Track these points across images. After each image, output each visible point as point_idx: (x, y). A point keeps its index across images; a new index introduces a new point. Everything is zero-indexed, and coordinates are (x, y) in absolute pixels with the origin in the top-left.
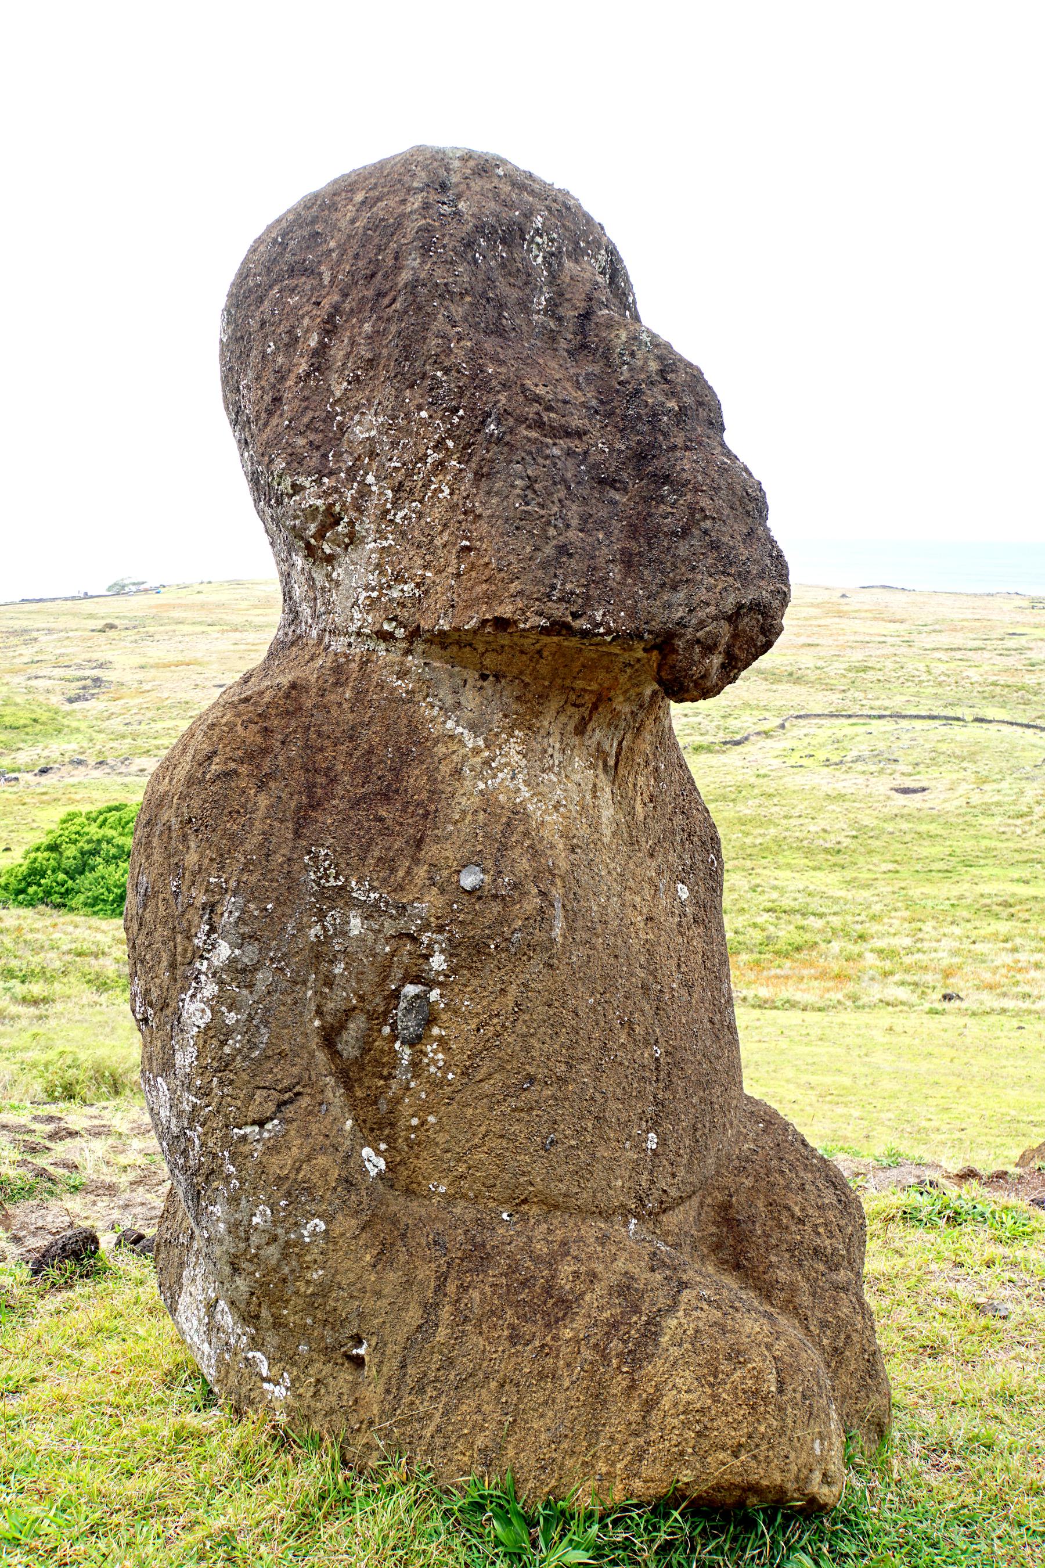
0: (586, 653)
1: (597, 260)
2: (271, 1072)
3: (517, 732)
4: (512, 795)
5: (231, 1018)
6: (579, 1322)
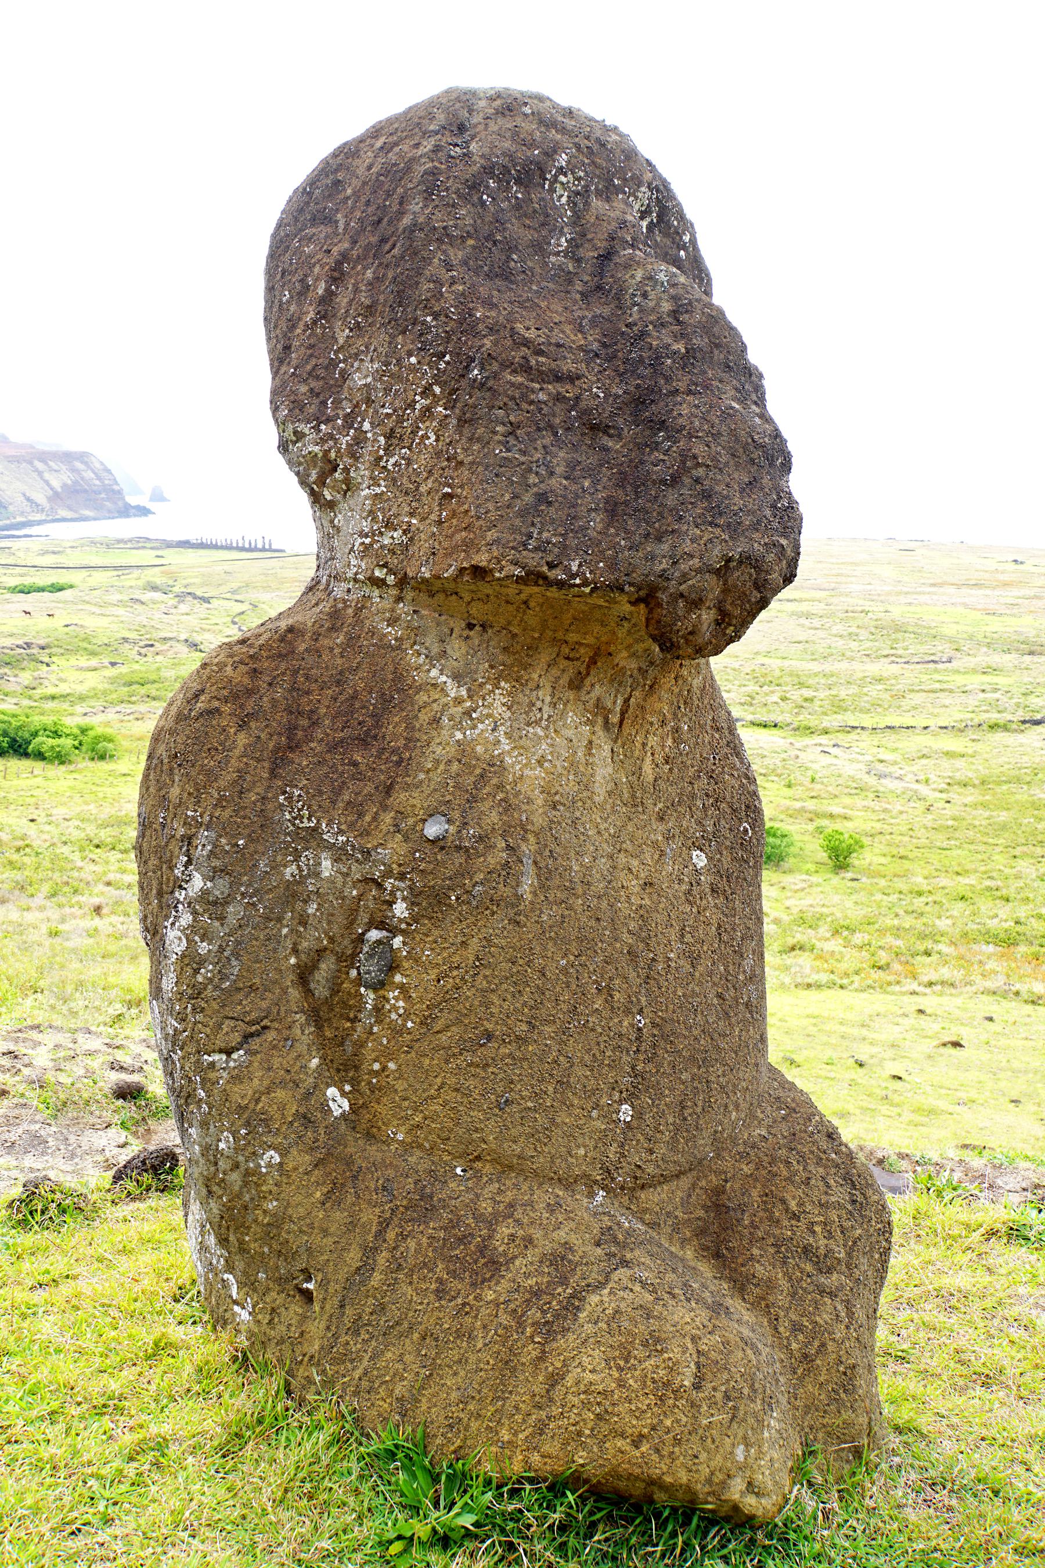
0: (575, 605)
1: (636, 198)
2: (240, 1004)
3: (503, 684)
4: (490, 747)
5: (204, 948)
6: (505, 1285)
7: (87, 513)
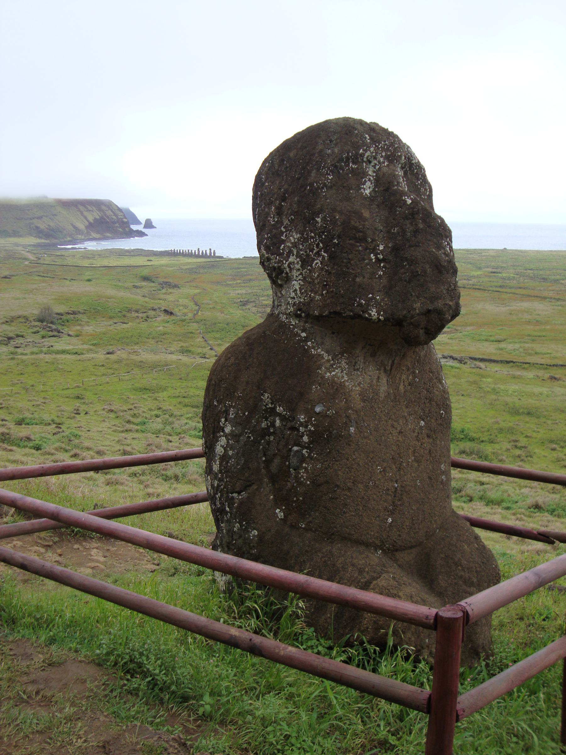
5: (230, 453)
7: (108, 235)
